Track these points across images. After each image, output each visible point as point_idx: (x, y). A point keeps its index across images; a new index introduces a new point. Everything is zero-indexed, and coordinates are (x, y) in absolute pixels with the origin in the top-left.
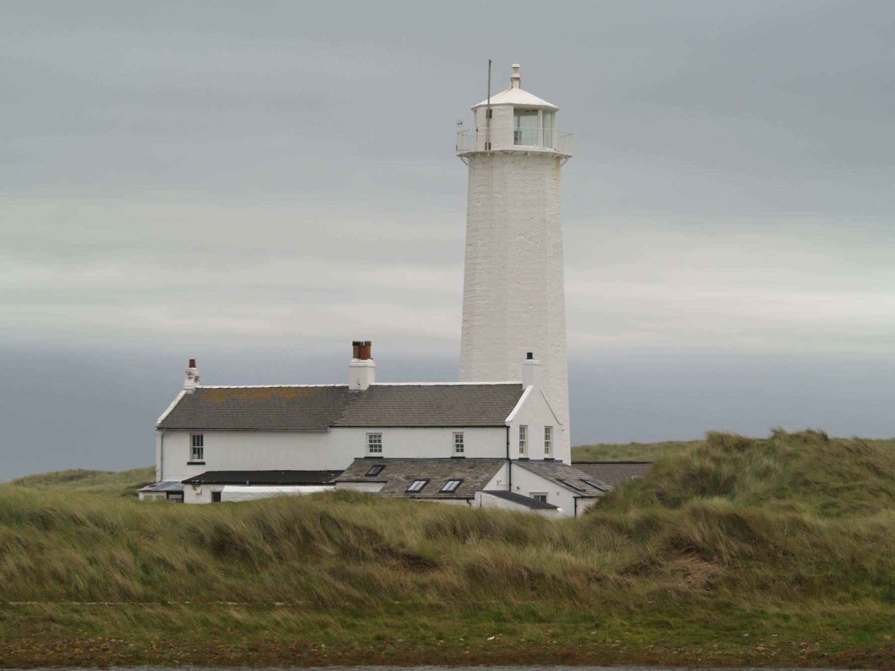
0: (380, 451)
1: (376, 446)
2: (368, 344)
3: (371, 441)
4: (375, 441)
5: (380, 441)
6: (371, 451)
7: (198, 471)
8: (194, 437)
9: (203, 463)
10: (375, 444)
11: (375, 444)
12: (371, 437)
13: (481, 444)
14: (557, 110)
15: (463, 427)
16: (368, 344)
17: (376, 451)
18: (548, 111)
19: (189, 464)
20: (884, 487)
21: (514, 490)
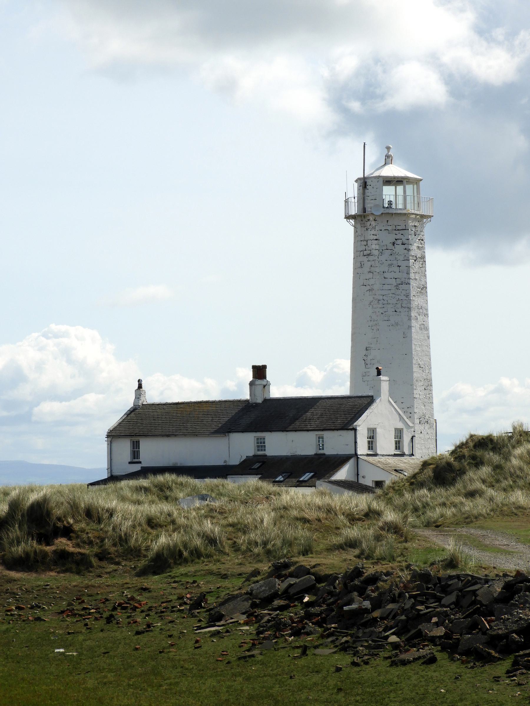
0: (265, 450)
1: (262, 446)
2: (264, 367)
3: (258, 443)
4: (261, 443)
5: (264, 443)
6: (258, 450)
7: (136, 468)
8: (133, 442)
9: (140, 462)
10: (261, 444)
11: (261, 444)
12: (257, 439)
13: (334, 443)
14: (421, 180)
15: (323, 430)
16: (264, 367)
17: (262, 450)
18: (416, 182)
19: (130, 463)
20: (298, 516)
21: (361, 481)
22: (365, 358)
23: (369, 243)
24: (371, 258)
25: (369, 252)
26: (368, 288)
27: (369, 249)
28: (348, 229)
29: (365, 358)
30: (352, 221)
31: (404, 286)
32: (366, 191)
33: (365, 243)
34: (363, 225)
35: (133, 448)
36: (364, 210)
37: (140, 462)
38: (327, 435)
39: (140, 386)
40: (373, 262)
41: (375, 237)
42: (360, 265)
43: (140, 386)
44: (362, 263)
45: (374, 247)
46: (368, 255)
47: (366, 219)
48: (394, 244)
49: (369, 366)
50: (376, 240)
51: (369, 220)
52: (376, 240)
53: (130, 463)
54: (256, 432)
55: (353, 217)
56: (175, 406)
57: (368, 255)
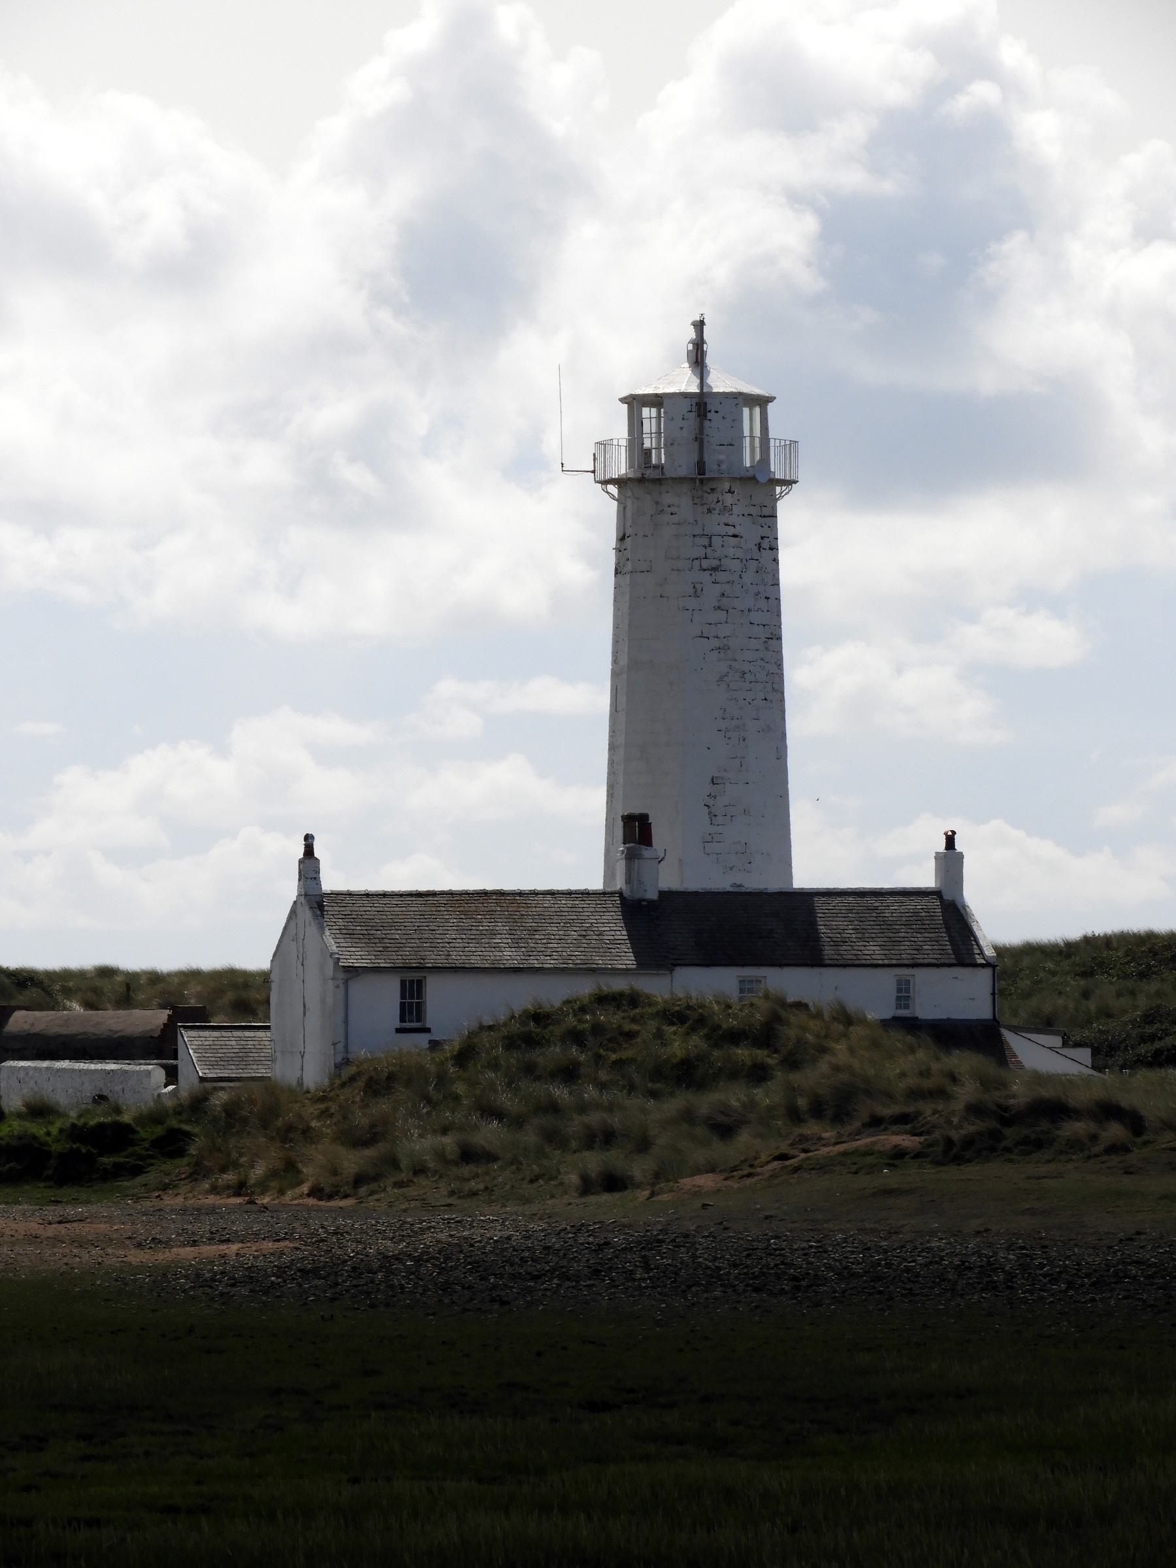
9: (428, 1030)
11: (904, 995)
12: (741, 982)
19: (398, 1031)
22: (710, 802)
23: (717, 541)
24: (721, 576)
25: (715, 563)
26: (715, 643)
27: (717, 555)
28: (605, 509)
29: (710, 802)
30: (613, 489)
31: (774, 642)
32: (707, 424)
33: (705, 541)
34: (697, 501)
35: (403, 996)
36: (701, 466)
37: (428, 1030)
38: (921, 976)
39: (309, 851)
40: (727, 587)
41: (731, 531)
42: (692, 591)
43: (309, 851)
44: (699, 587)
45: (731, 552)
46: (715, 569)
47: (707, 488)
48: (759, 547)
49: (720, 820)
50: (735, 536)
51: (713, 490)
52: (735, 536)
53: (398, 1031)
54: (743, 965)
55: (619, 482)
56: (417, 905)
57: (715, 569)
